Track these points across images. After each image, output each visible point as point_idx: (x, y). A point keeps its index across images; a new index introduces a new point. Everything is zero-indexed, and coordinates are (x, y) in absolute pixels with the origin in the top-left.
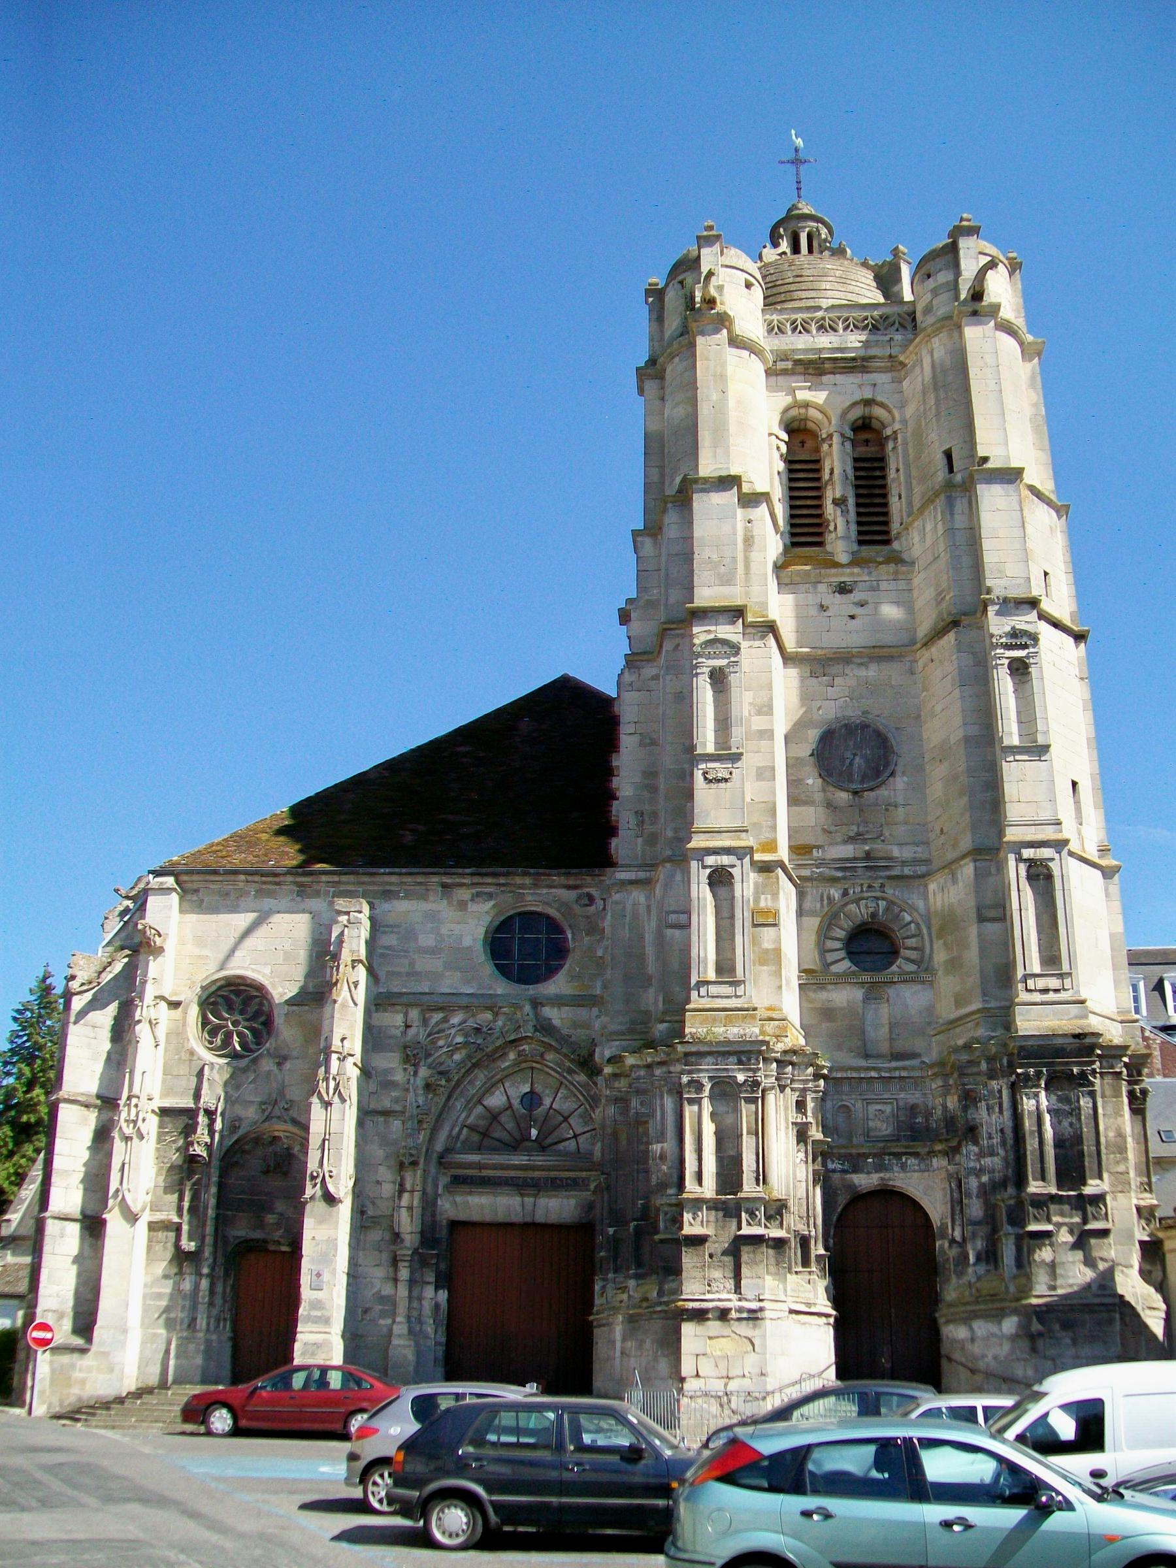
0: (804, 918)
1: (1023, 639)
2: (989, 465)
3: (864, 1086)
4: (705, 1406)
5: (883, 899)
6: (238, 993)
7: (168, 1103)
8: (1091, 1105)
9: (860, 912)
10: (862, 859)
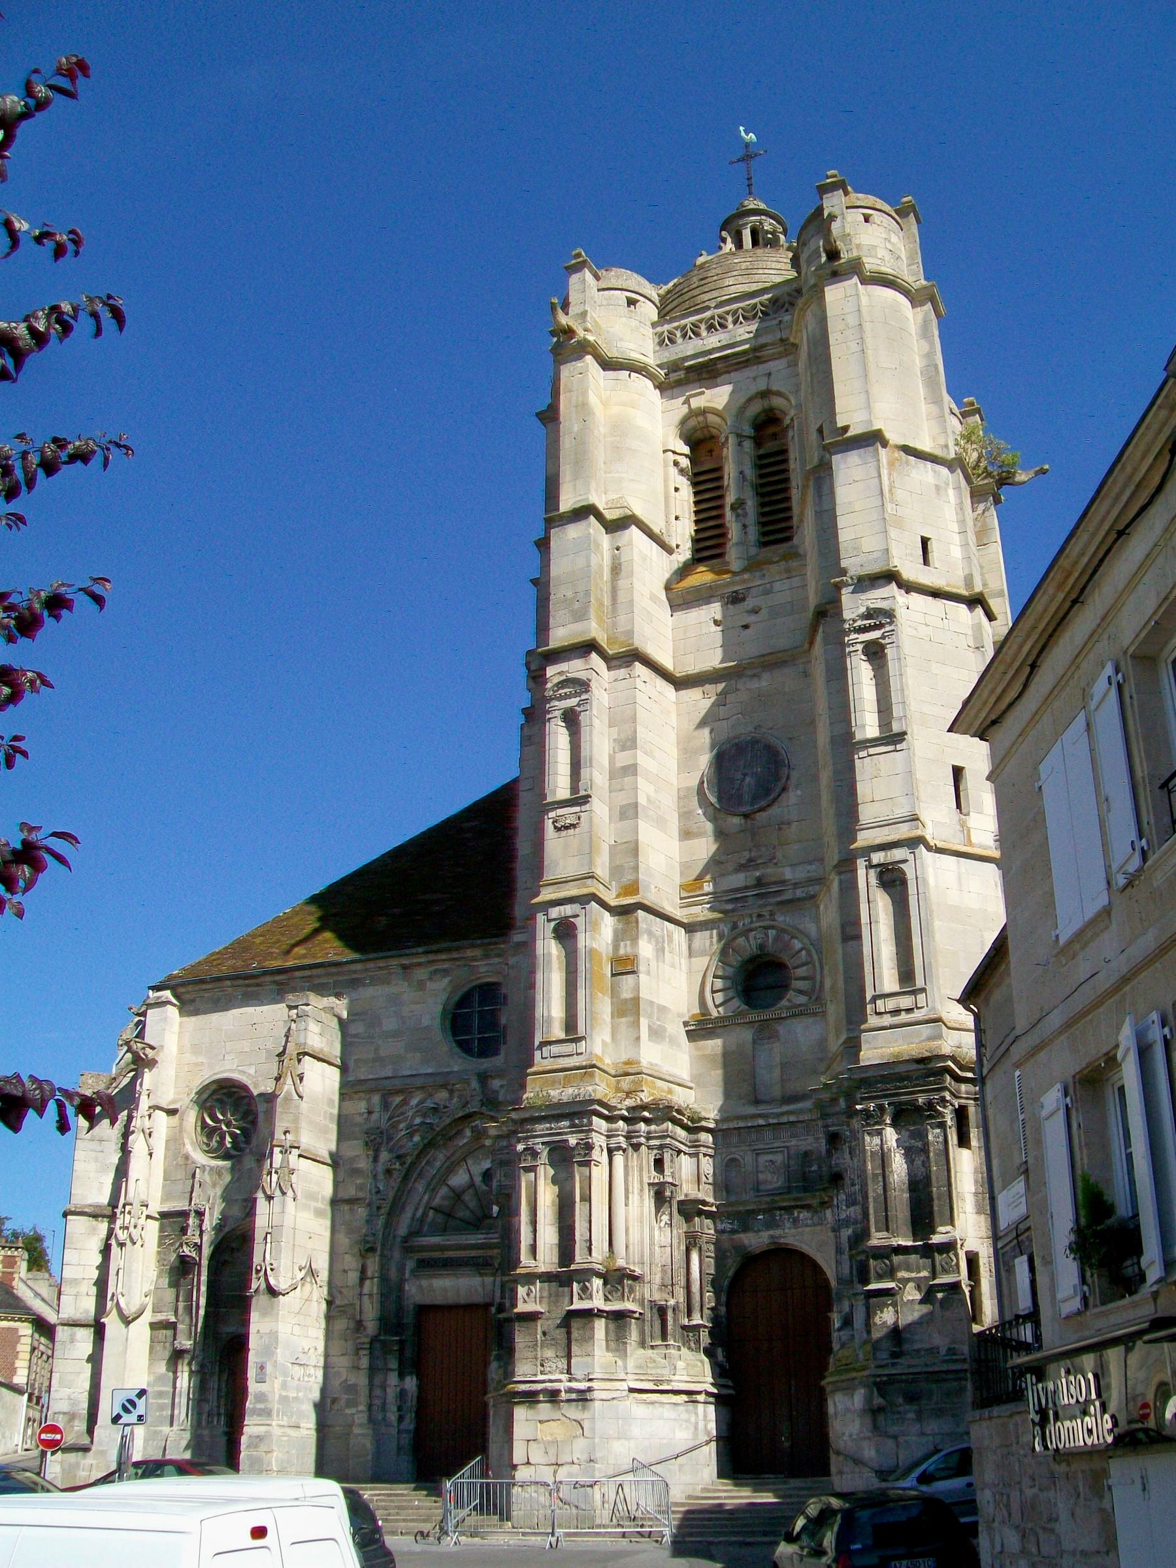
0: (693, 960)
1: (881, 617)
2: (849, 434)
3: (754, 1137)
4: (534, 1495)
5: (772, 927)
6: (230, 1095)
7: (166, 1208)
8: (941, 1139)
9: (748, 946)
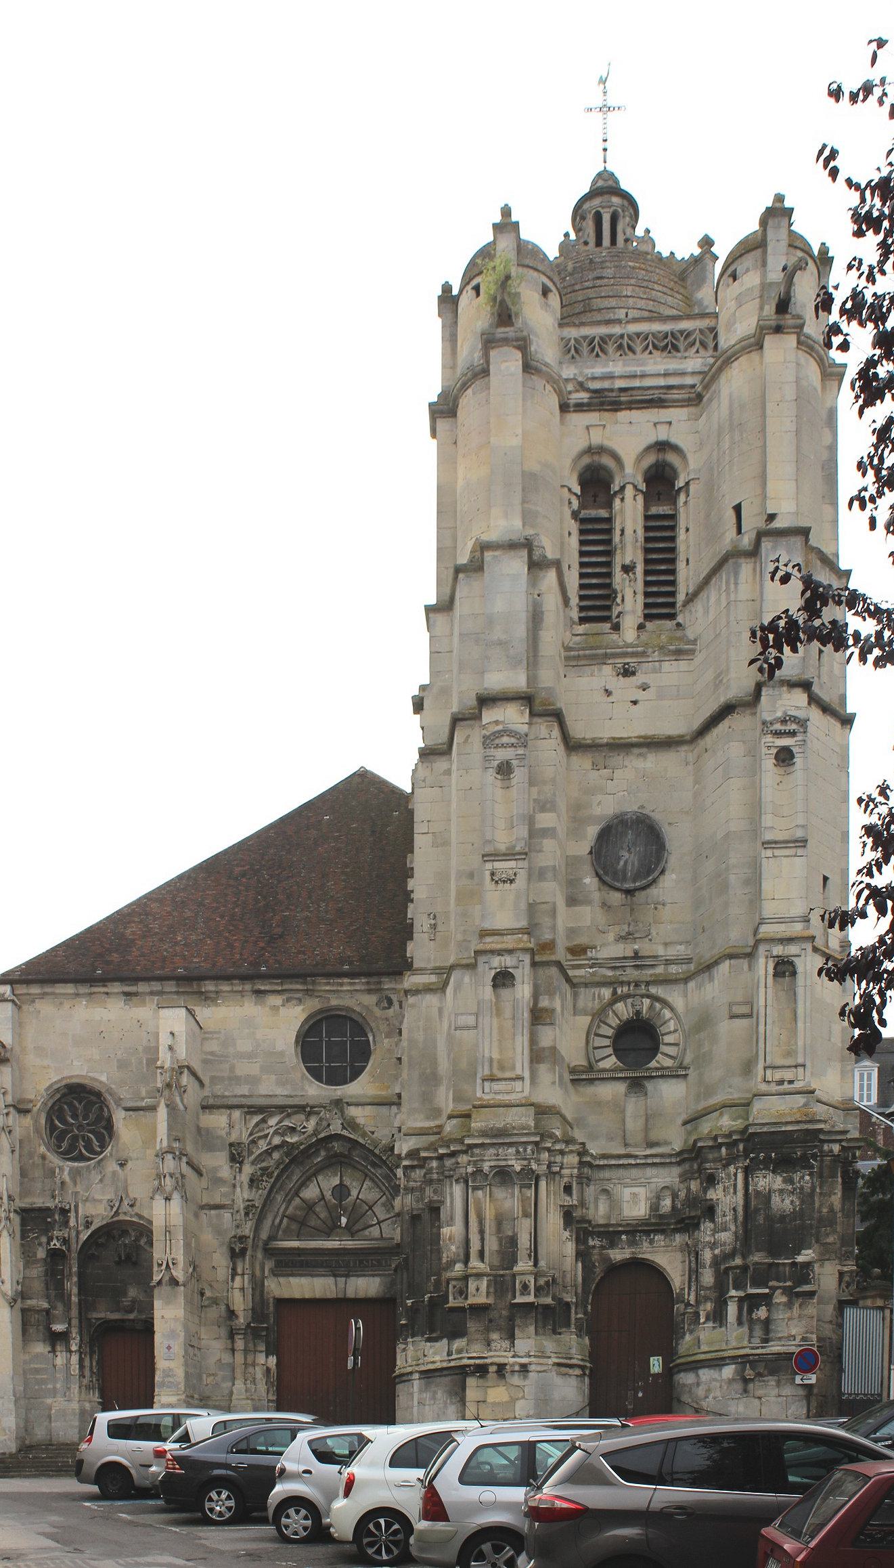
10: (632, 958)
